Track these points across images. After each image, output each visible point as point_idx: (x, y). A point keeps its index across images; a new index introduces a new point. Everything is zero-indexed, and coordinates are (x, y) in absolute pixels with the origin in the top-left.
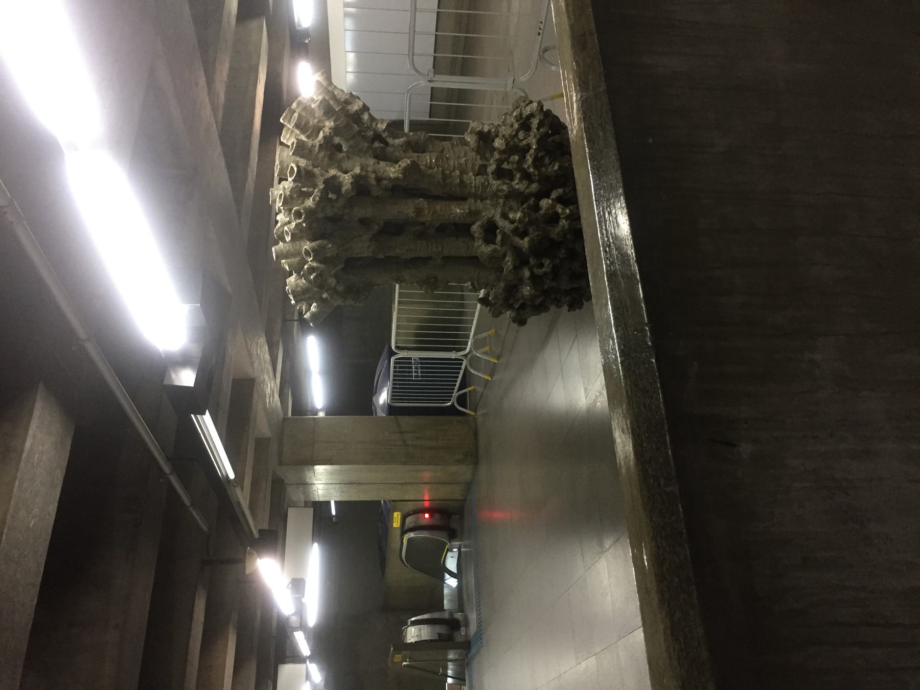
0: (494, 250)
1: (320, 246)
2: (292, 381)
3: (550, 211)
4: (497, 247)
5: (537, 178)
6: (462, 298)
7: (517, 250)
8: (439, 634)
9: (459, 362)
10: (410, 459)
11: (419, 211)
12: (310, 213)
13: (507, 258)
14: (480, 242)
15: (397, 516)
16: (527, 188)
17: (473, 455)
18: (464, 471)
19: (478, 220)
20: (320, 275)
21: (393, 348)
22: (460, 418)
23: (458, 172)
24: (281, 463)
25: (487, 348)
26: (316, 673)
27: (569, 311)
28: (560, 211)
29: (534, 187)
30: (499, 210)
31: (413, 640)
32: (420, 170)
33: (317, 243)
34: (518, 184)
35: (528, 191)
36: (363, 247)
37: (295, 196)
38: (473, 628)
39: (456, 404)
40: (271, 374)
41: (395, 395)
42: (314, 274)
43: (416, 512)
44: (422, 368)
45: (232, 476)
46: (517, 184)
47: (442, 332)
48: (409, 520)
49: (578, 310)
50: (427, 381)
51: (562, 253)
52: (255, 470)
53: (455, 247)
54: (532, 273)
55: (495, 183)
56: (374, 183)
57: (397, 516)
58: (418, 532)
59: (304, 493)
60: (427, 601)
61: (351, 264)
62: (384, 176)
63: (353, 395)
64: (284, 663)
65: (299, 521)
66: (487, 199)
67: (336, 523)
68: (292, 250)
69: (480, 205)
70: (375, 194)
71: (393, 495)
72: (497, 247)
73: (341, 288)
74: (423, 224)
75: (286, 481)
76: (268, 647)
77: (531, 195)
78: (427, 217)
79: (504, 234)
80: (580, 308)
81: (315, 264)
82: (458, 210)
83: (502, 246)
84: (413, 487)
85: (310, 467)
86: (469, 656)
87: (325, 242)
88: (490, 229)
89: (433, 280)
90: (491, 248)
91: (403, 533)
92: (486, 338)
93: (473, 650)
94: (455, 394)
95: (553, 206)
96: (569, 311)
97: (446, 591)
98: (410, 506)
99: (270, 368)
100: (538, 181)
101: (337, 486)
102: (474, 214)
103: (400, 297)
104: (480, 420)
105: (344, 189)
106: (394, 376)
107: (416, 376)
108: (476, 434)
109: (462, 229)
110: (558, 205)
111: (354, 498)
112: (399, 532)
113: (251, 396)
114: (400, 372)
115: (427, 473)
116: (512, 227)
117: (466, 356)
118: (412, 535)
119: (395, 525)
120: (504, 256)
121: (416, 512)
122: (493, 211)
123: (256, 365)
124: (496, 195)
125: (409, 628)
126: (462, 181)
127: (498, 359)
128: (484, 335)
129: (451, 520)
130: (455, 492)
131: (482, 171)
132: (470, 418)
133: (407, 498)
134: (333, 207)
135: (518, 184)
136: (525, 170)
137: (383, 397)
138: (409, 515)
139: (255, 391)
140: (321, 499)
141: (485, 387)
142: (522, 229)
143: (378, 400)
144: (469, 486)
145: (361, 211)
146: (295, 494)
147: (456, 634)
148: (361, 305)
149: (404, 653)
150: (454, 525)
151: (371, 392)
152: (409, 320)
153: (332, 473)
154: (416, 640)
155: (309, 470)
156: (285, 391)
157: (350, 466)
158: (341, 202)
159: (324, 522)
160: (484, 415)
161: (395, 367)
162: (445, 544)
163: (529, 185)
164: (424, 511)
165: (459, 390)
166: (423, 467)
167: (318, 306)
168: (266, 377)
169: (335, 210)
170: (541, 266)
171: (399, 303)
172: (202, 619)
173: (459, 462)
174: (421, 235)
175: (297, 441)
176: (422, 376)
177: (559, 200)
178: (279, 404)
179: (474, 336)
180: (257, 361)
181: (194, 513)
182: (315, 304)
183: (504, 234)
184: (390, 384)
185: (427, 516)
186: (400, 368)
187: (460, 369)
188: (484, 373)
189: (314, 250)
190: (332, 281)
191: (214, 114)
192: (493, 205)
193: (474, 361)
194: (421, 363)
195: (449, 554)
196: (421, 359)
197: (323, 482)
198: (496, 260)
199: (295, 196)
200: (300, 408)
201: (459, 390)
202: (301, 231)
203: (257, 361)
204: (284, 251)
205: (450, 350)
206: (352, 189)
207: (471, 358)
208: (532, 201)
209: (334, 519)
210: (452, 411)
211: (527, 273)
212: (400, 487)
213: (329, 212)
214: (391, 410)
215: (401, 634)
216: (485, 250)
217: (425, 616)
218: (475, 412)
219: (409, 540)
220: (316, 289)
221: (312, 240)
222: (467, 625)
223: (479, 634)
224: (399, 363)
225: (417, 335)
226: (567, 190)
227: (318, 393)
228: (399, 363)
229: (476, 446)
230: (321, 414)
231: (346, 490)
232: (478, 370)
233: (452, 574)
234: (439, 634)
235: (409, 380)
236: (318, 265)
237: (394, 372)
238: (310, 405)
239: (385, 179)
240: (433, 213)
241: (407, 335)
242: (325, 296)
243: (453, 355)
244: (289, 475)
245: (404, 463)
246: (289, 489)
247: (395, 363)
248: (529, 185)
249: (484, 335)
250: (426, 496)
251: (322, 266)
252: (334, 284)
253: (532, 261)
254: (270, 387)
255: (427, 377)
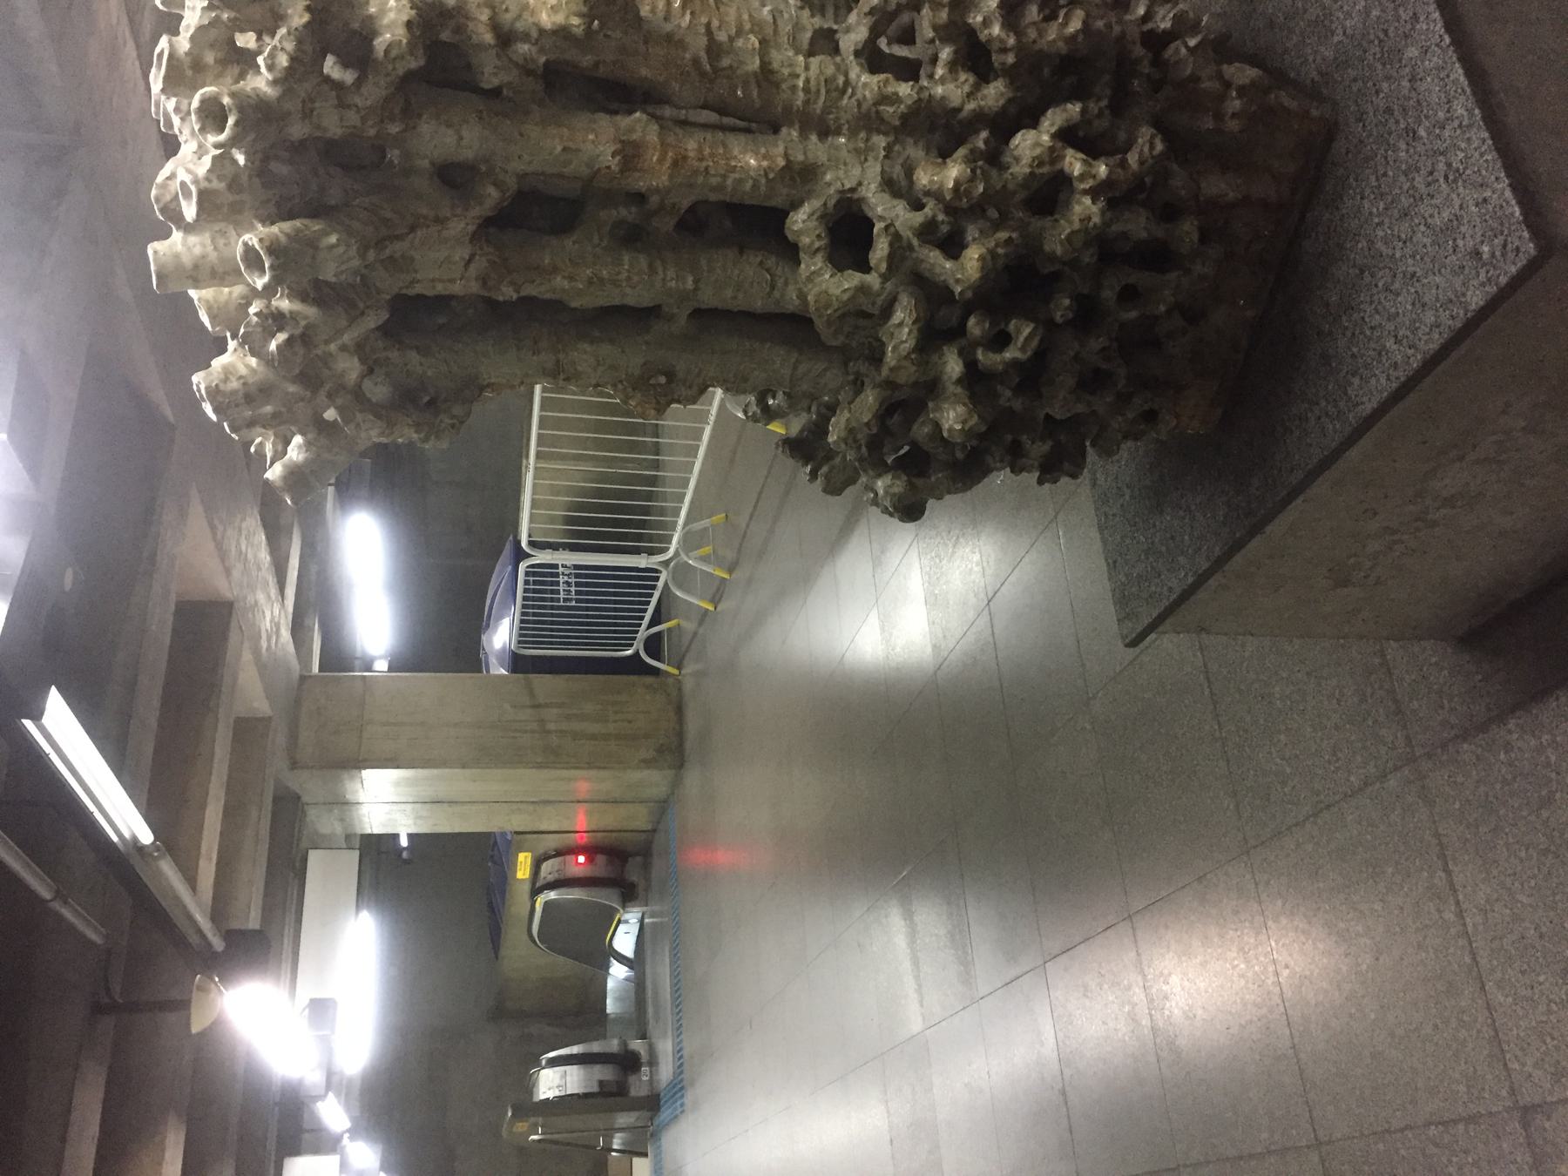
0: (862, 289)
1: (294, 237)
2: (318, 603)
3: (1045, 169)
4: (873, 280)
5: (1010, 59)
6: (657, 449)
7: (932, 293)
8: (601, 1083)
9: (651, 575)
10: (552, 756)
11: (630, 153)
12: (257, 115)
13: (899, 315)
14: (819, 262)
15: (524, 861)
16: (970, 95)
17: (674, 752)
18: (654, 781)
19: (809, 195)
20: (303, 340)
21: (524, 544)
22: (649, 680)
23: (754, 40)
24: (294, 765)
25: (707, 550)
26: (365, 1155)
27: (1040, 482)
28: (1077, 169)
29: (995, 94)
30: (874, 170)
31: (550, 1094)
32: (639, 19)
33: (287, 226)
34: (949, 87)
35: (971, 106)
36: (446, 261)
37: (210, 58)
38: (665, 1072)
39: (643, 654)
40: (273, 591)
41: (527, 631)
42: (281, 337)
43: (559, 853)
44: (577, 584)
45: (146, 837)
46: (943, 80)
47: (617, 515)
48: (546, 867)
49: (1064, 480)
50: (587, 609)
51: (1062, 307)
52: (230, 789)
53: (738, 279)
54: (971, 365)
55: (868, 83)
56: (488, 38)
57: (524, 861)
58: (563, 890)
59: (342, 820)
60: (572, 1013)
61: (412, 317)
62: (519, 26)
63: (443, 637)
64: (296, 1152)
65: (329, 876)
66: (838, 133)
67: (406, 862)
68: (213, 256)
69: (816, 149)
70: (490, 80)
71: (516, 822)
72: (873, 280)
73: (378, 391)
74: (640, 198)
75: (305, 799)
76: (253, 1135)
77: (980, 119)
78: (656, 175)
79: (896, 238)
80: (1074, 476)
81: (284, 304)
82: (751, 160)
83: (885, 278)
84: (551, 810)
85: (355, 772)
86: (656, 1122)
87: (317, 226)
88: (849, 232)
89: (663, 380)
90: (852, 279)
91: (536, 892)
92: (706, 529)
93: (664, 1115)
94: (643, 633)
95: (1053, 156)
96: (1040, 482)
97: (610, 984)
98: (552, 842)
99: (272, 581)
100: (1011, 73)
101: (409, 807)
102: (802, 176)
103: (539, 444)
104: (688, 685)
105: (382, 42)
106: (525, 599)
107: (565, 600)
108: (679, 710)
109: (757, 224)
110: (1070, 152)
111: (445, 828)
112: (527, 887)
113: (224, 636)
114: (535, 591)
115: (584, 783)
116: (918, 218)
117: (666, 563)
118: (552, 895)
119: (520, 875)
120: (887, 311)
121: (559, 853)
122: (856, 171)
123: (236, 574)
124: (869, 121)
125: (544, 1072)
126: (766, 68)
127: (730, 571)
128: (705, 523)
129: (624, 866)
130: (640, 818)
131: (825, 42)
132: (670, 680)
133: (544, 827)
134: (342, 105)
135: (949, 87)
136: (971, 32)
137: (501, 636)
138: (547, 857)
139: (234, 624)
140: (376, 831)
141: (701, 623)
142: (945, 229)
143: (490, 642)
144: (662, 807)
145: (444, 137)
146: (324, 823)
147: (632, 1079)
148: (444, 445)
149: (533, 1120)
150: (633, 875)
151: (476, 623)
152: (555, 491)
153: (397, 784)
154: (557, 1093)
155: (352, 778)
156: (307, 622)
157: (435, 771)
158: (374, 92)
159: (385, 867)
160: (699, 675)
161: (526, 582)
162: (613, 911)
163: (976, 88)
164: (574, 851)
165: (650, 626)
166: (573, 773)
167: (308, 445)
168: (261, 597)
169: (353, 118)
170: (1001, 340)
171: (539, 455)
172: (94, 1129)
173: (647, 763)
174: (632, 237)
175: (332, 721)
176: (577, 601)
177: (1067, 136)
178: (291, 648)
179: (685, 524)
180: (240, 566)
181: (66, 913)
182: (298, 440)
183: (896, 238)
184: (516, 611)
185: (581, 859)
186: (535, 583)
187: (654, 587)
188: (702, 598)
189: (273, 249)
190: (350, 368)
191: (131, 21)
192: (857, 151)
193: (683, 574)
194: (577, 576)
195: (622, 928)
196: (576, 567)
197: (385, 801)
198: (865, 317)
199: (210, 58)
200: (338, 658)
201: (650, 626)
202: (234, 184)
203: (240, 566)
204: (187, 260)
205: (636, 551)
206: (412, 45)
207: (676, 565)
208: (981, 140)
209: (405, 855)
210: (634, 666)
211: (953, 366)
212: (531, 808)
213: (333, 124)
214: (518, 663)
215: (529, 1086)
216: (824, 284)
217: (575, 1050)
218: (679, 668)
219: (547, 904)
220: (292, 388)
221: (269, 220)
222: (653, 1062)
223: (678, 1087)
224: (534, 574)
225: (569, 521)
226: (1093, 107)
227: (375, 621)
228: (534, 574)
229: (680, 735)
230: (381, 666)
231: (424, 814)
232: (688, 591)
233: (622, 959)
234: (601, 1083)
235: (552, 608)
236: (297, 306)
237: (526, 591)
238: (359, 648)
239: (526, 37)
240: (675, 163)
241: (552, 520)
242: (330, 414)
243: (642, 561)
244: (309, 786)
245: (540, 766)
246: (312, 813)
247: (527, 574)
248: (976, 88)
249: (705, 523)
250: (581, 821)
251: (311, 311)
252: (353, 376)
253: (975, 326)
254: (271, 615)
255: (588, 601)
